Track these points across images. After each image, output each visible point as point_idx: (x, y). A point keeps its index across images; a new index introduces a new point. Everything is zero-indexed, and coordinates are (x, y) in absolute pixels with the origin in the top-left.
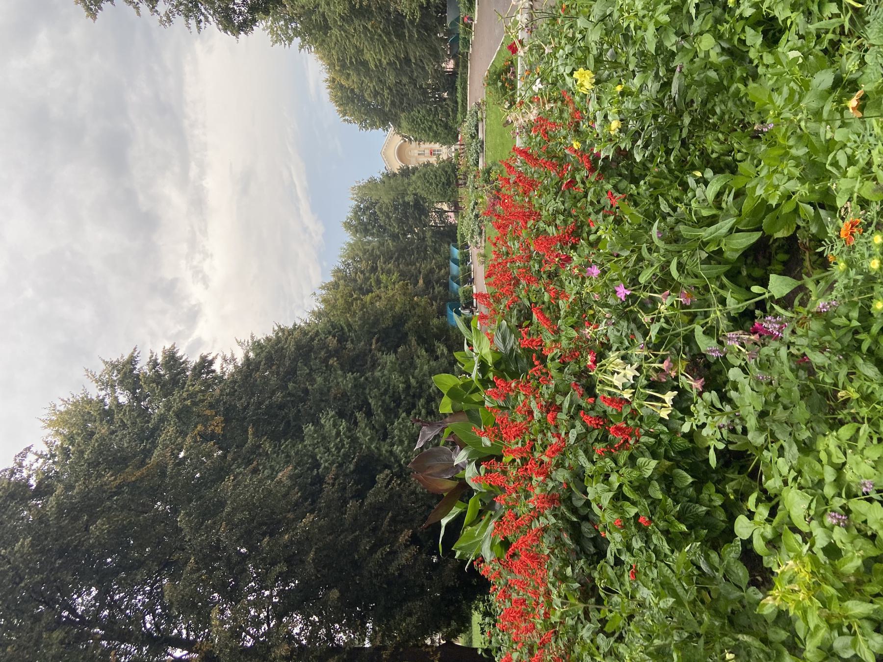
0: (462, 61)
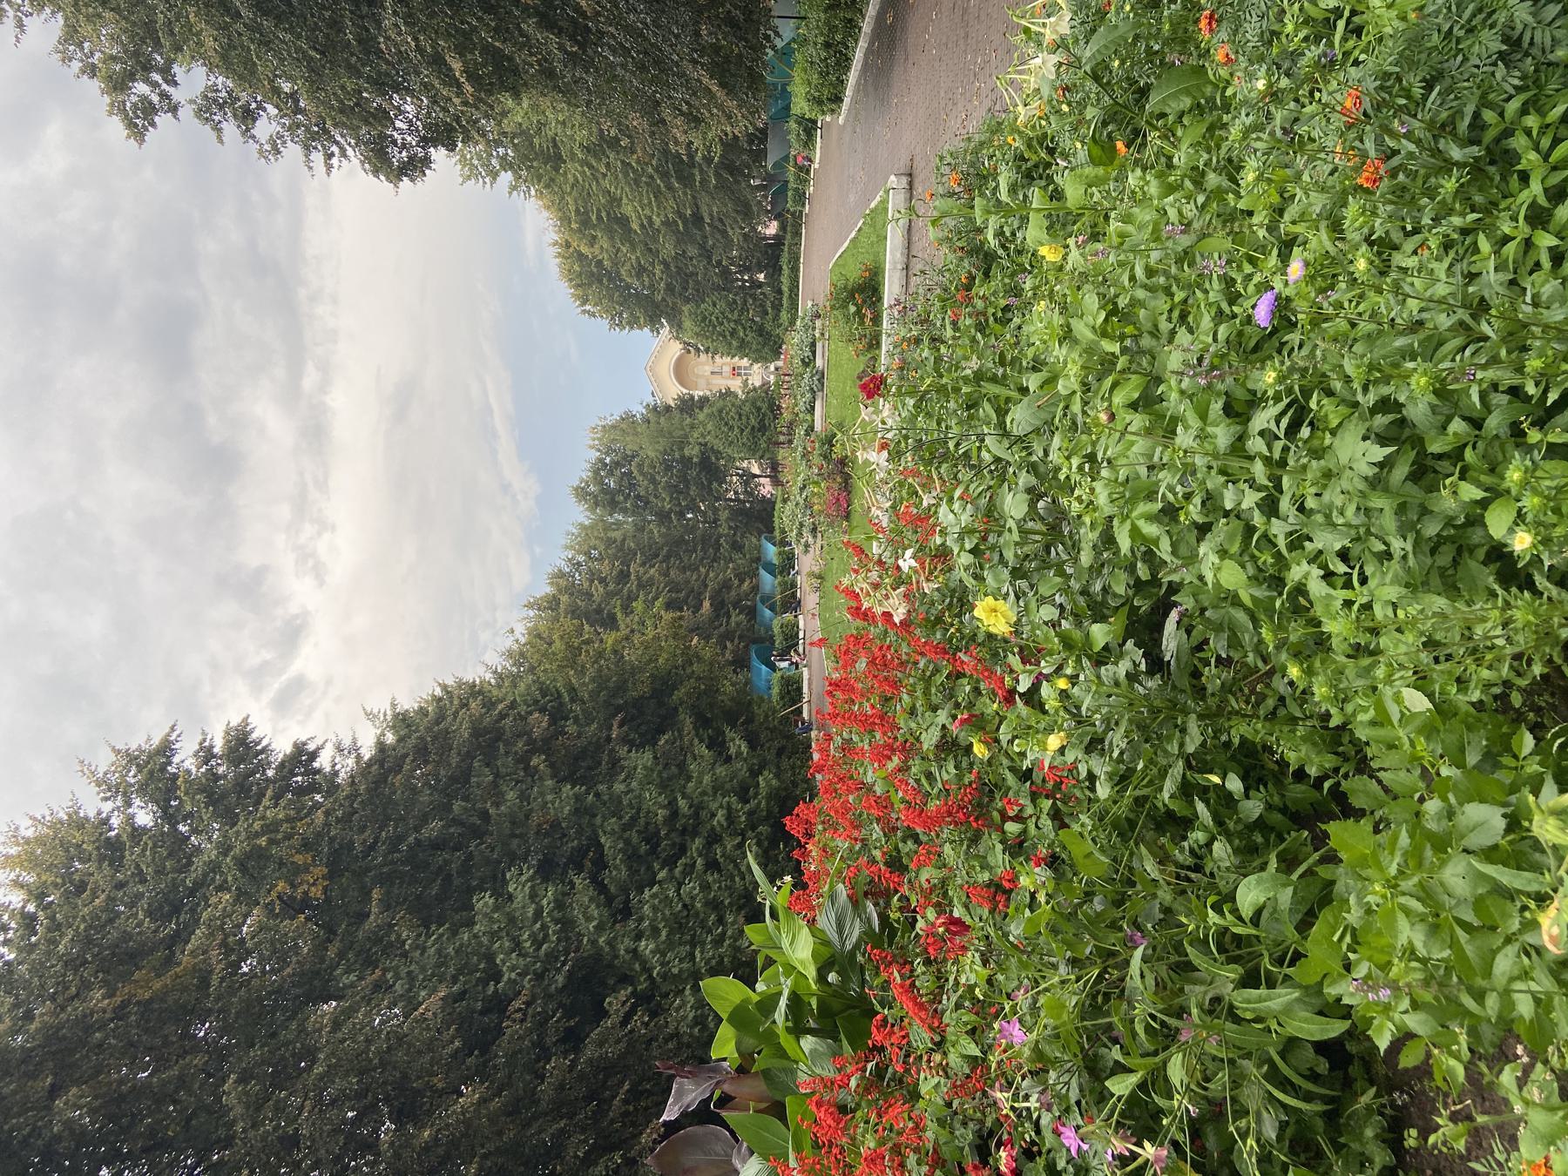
0: (792, 225)
